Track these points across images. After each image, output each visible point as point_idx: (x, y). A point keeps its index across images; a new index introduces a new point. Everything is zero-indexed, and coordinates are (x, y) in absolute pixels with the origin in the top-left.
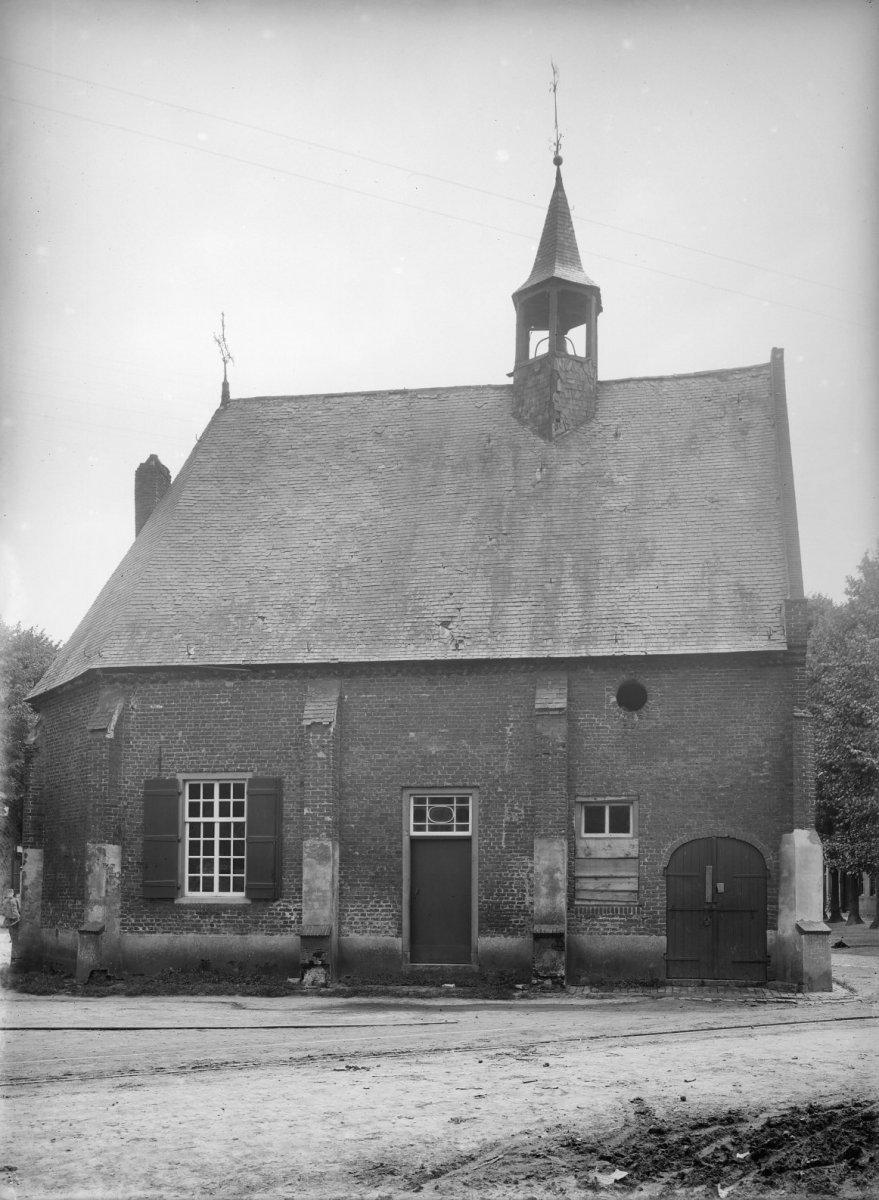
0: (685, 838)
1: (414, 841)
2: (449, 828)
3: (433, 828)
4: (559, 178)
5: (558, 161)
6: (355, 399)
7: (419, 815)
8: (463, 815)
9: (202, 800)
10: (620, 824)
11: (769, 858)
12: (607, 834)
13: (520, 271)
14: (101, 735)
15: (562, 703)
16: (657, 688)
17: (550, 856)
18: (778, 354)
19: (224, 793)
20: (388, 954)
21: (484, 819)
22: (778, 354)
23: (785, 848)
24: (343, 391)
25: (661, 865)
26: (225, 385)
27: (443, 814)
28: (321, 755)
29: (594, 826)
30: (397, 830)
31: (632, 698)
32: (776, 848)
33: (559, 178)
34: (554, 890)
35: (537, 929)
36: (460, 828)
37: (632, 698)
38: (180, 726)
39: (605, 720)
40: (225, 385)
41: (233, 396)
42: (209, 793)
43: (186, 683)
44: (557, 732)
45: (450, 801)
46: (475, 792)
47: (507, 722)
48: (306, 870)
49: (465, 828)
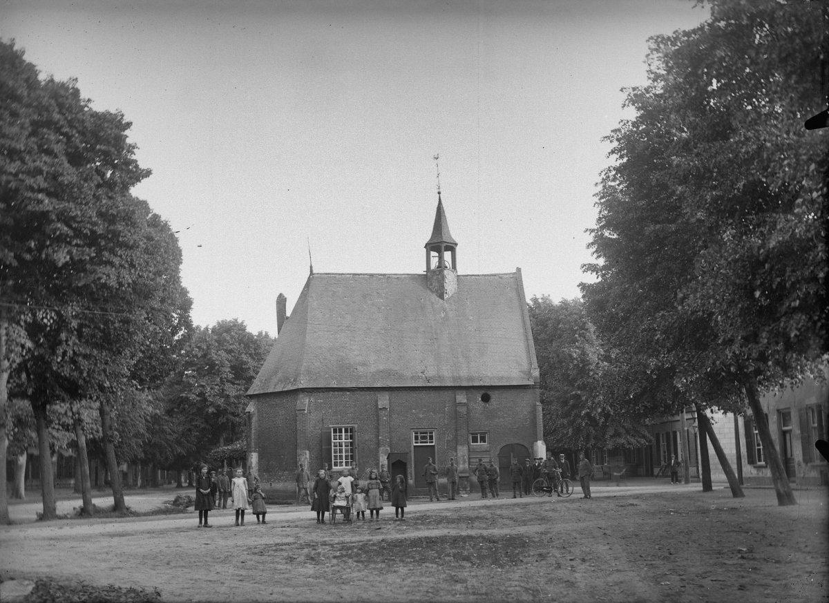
0: (503, 445)
1: (415, 446)
2: (427, 442)
3: (421, 442)
4: (440, 199)
5: (439, 193)
6: (603, 505)
7: (416, 438)
8: (431, 438)
9: (338, 434)
10: (483, 439)
11: (530, 450)
12: (479, 443)
13: (427, 235)
14: (302, 412)
15: (465, 401)
16: (494, 396)
17: (462, 451)
18: (519, 270)
19: (346, 431)
20: (439, 477)
21: (439, 439)
22: (519, 270)
23: (535, 448)
24: (360, 272)
25: (498, 453)
26: (311, 267)
27: (424, 438)
28: (385, 418)
29: (475, 440)
30: (410, 443)
31: (486, 398)
32: (532, 447)
33: (440, 199)
34: (464, 462)
35: (460, 475)
36: (430, 442)
37: (486, 398)
38: (330, 408)
39: (477, 404)
40: (311, 267)
41: (314, 272)
42: (341, 431)
43: (332, 393)
44: (463, 410)
45: (427, 433)
46: (436, 430)
47: (445, 407)
48: (381, 458)
49: (432, 442)
